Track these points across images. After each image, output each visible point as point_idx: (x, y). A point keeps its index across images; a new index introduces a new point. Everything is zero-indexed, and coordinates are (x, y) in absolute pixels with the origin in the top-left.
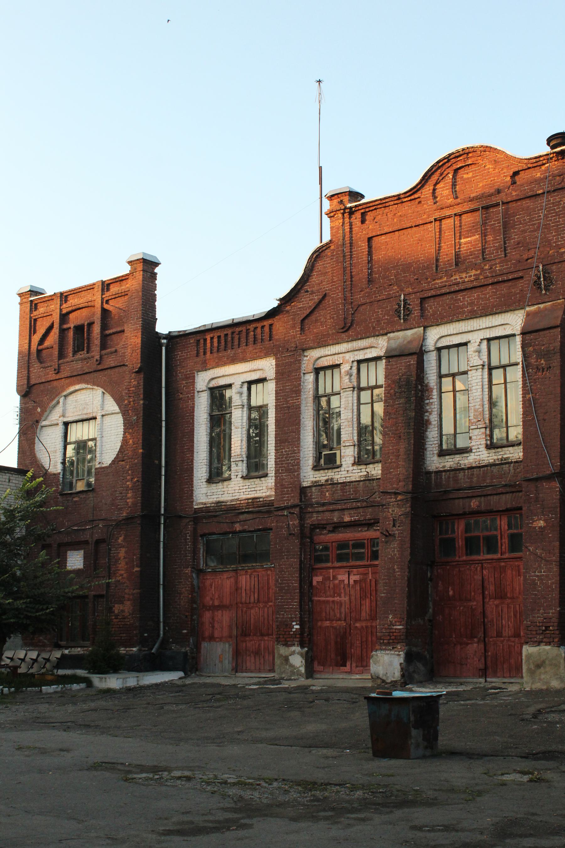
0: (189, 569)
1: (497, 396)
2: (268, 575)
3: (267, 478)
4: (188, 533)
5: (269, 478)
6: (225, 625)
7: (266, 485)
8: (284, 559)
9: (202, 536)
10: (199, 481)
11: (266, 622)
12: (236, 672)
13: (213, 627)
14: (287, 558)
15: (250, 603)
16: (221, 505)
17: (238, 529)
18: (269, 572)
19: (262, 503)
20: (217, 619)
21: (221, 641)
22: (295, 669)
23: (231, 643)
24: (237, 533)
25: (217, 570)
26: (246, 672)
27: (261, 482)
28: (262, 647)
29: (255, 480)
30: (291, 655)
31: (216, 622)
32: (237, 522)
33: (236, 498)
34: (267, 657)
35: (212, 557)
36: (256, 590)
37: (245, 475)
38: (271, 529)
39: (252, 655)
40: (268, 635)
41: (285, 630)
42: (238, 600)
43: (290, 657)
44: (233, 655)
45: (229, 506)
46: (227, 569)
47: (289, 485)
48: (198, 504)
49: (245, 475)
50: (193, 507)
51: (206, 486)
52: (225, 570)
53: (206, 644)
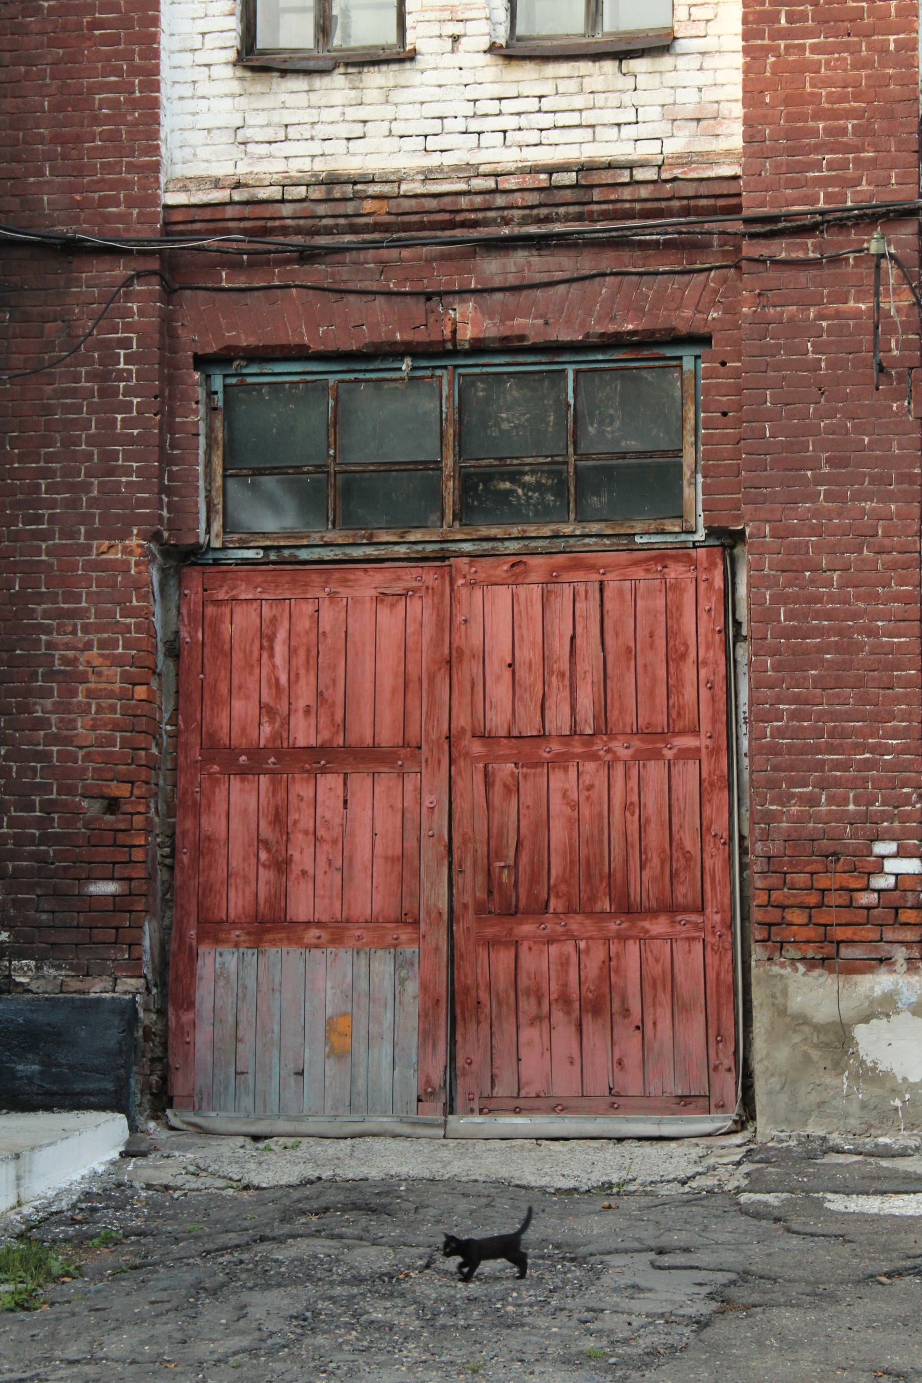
0: (134, 542)
1: (415, 50)
2: (676, 588)
3: (666, 62)
4: (125, 343)
5: (682, 62)
6: (363, 854)
7: (666, 96)
8: (814, 498)
9: (202, 362)
10: (187, 59)
11: (655, 836)
12: (450, 1109)
13: (282, 865)
14: (829, 496)
15: (542, 736)
16: (360, 197)
17: (467, 333)
18: (675, 571)
19: (644, 192)
20: (306, 822)
21: (337, 940)
22: (895, 1092)
23: (410, 951)
24: (455, 353)
25: (304, 554)
26: (517, 1111)
27: (629, 82)
28: (633, 975)
29: (585, 67)
30: (866, 1020)
31: (298, 838)
32: (464, 292)
33: (449, 160)
34: (665, 1025)
35: (269, 482)
36: (590, 661)
37: (502, 41)
38: (704, 340)
39: (558, 1016)
40: (671, 909)
41: (823, 881)
42: (463, 720)
43: (861, 1032)
44: (424, 1015)
45: (407, 204)
46: (370, 551)
47: (842, 99)
48: (184, 184)
49: (502, 41)
50: (154, 200)
51: (235, 87)
52: (357, 553)
53: (230, 959)
